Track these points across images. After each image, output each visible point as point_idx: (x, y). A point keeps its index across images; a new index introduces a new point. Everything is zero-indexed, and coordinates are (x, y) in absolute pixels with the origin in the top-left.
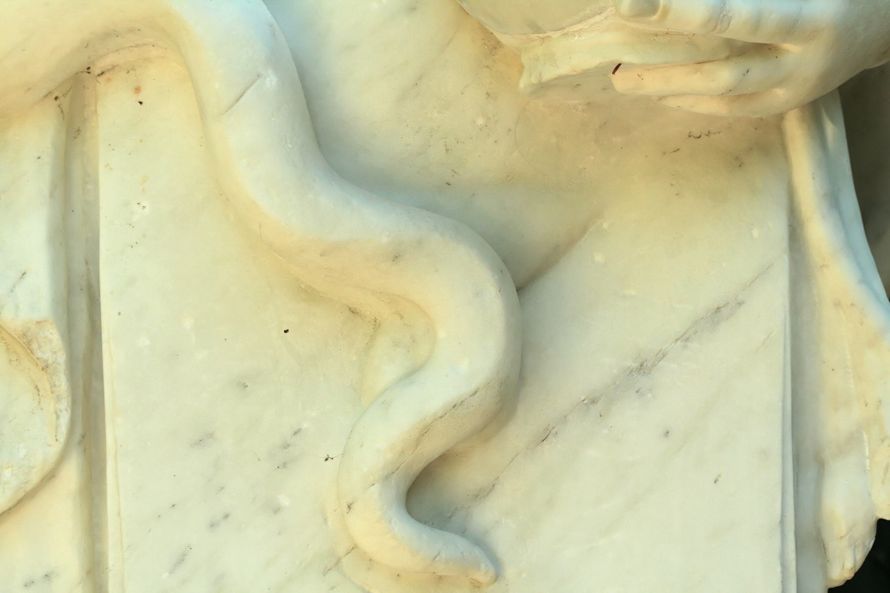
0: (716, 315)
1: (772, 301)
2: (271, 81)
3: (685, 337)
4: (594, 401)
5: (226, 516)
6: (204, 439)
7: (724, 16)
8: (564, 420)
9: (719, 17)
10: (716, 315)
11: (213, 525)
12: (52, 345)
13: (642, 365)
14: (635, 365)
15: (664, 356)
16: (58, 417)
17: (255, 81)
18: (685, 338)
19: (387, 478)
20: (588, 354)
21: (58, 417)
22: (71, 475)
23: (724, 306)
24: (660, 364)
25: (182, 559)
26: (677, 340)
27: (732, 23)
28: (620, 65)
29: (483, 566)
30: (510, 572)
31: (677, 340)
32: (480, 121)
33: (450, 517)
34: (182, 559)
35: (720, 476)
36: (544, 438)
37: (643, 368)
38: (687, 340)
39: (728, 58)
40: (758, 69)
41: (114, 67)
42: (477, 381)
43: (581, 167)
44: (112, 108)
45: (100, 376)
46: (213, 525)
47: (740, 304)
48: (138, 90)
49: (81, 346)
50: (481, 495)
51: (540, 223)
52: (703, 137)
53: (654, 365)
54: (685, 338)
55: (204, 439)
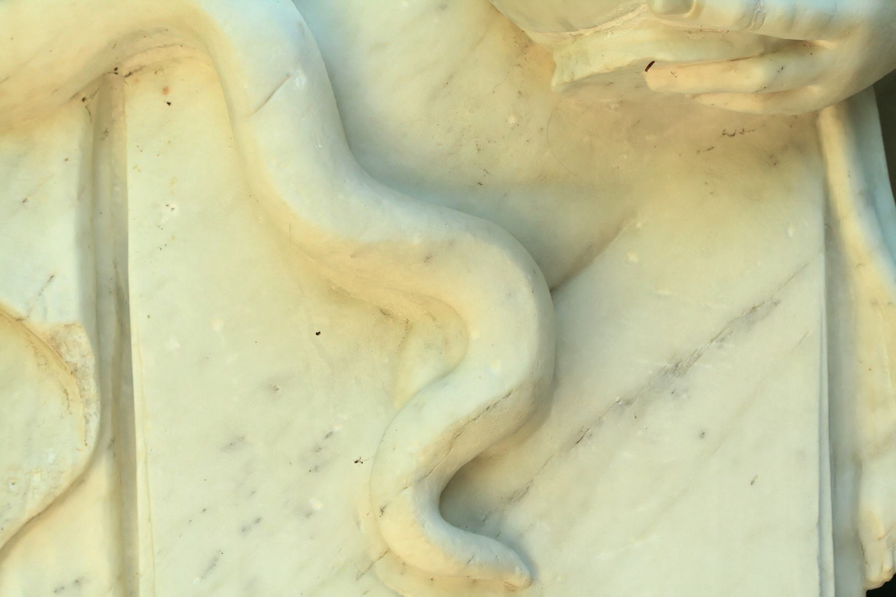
0: (752, 315)
1: (806, 305)
2: (300, 81)
4: (628, 403)
5: (258, 521)
6: (235, 443)
10: (752, 315)
11: (244, 530)
12: (81, 348)
13: (677, 366)
14: (670, 366)
15: (699, 356)
17: (284, 81)
18: (720, 339)
19: (420, 481)
20: (621, 356)
21: (87, 422)
22: (101, 480)
24: (696, 364)
25: (213, 564)
26: (712, 341)
27: (766, 19)
28: (653, 62)
29: (517, 569)
32: (512, 120)
34: (213, 564)
38: (723, 340)
39: (762, 55)
40: (793, 66)
41: (141, 68)
42: (510, 383)
44: (140, 109)
45: (130, 381)
46: (244, 530)
47: (776, 304)
48: (166, 90)
49: (110, 350)
50: (516, 497)
51: (573, 223)
52: (738, 135)
53: (689, 366)
54: (720, 339)
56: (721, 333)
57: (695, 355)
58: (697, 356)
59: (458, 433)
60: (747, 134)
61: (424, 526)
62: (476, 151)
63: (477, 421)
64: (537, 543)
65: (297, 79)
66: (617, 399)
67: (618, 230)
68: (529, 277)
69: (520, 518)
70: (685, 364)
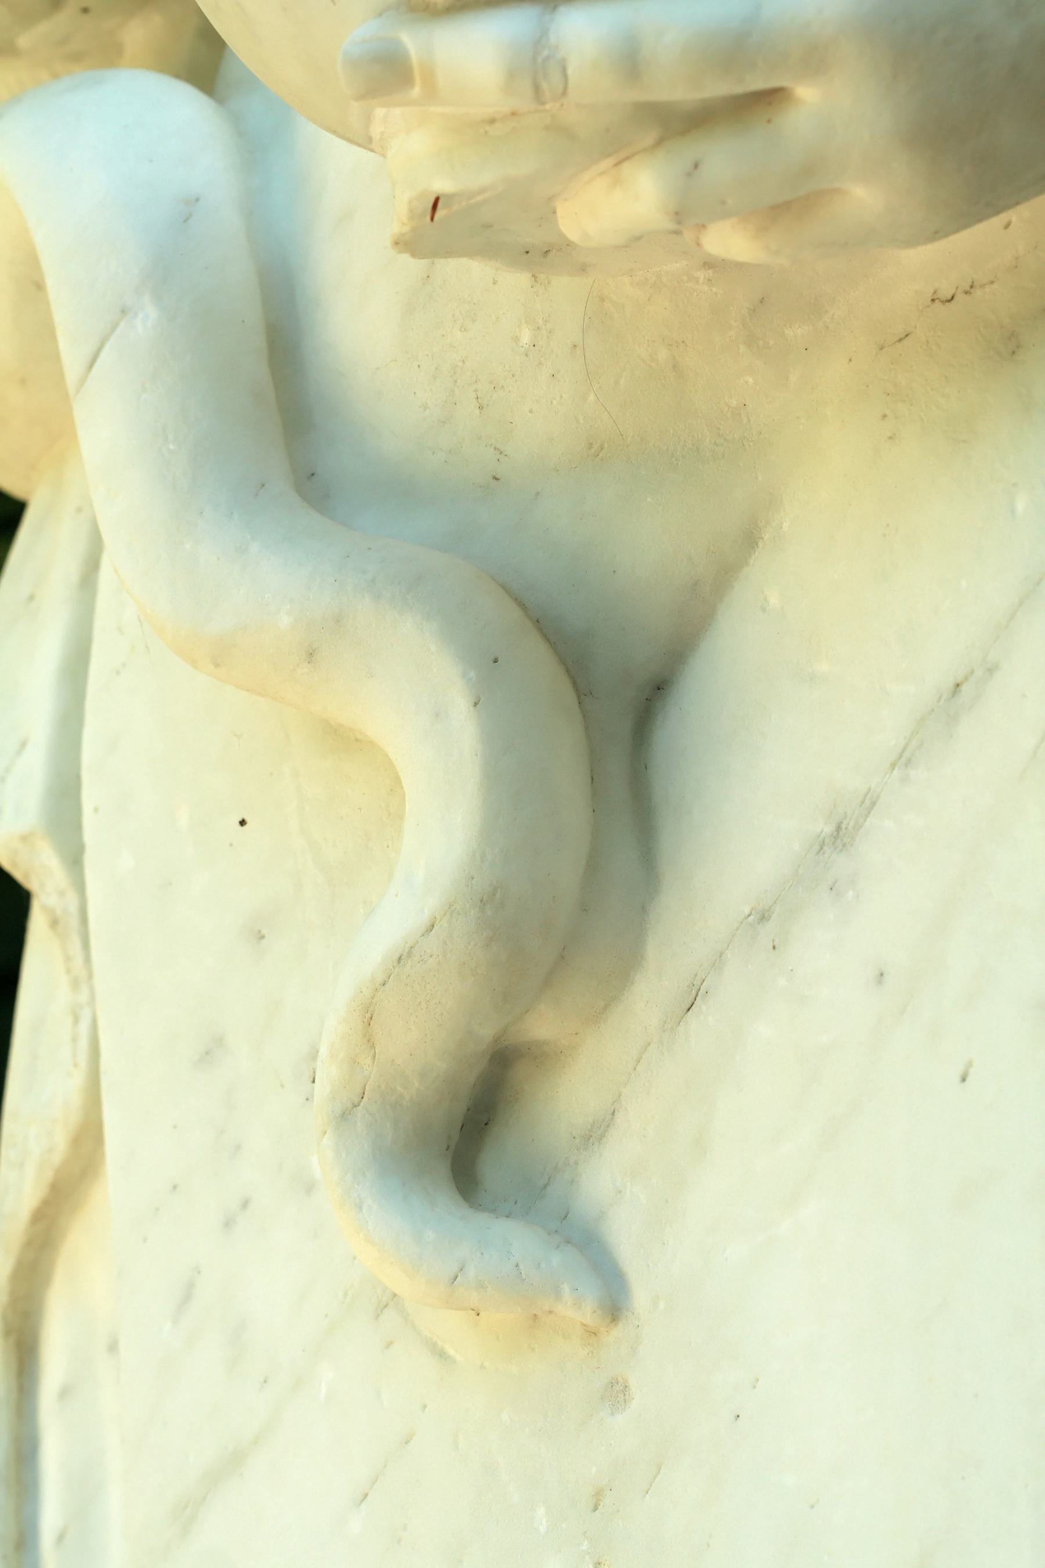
2: (147, 318)
3: (903, 760)
4: (764, 917)
5: (245, 1204)
7: (546, 60)
8: (718, 961)
9: (630, 61)
13: (839, 828)
14: (829, 829)
15: (874, 804)
16: (76, 1020)
17: (114, 327)
18: (903, 760)
19: (344, 1116)
21: (76, 1020)
23: (966, 679)
24: (867, 823)
25: (187, 1297)
26: (893, 766)
27: (570, 71)
28: (437, 200)
29: (566, 1288)
30: (641, 1296)
31: (893, 766)
32: (526, 337)
33: (545, 1187)
34: (187, 1297)
35: (970, 1064)
36: (691, 1001)
37: (840, 836)
38: (908, 763)
39: (659, 143)
42: (431, 905)
43: (734, 403)
46: (228, 1224)
47: (991, 670)
50: (594, 1135)
51: (647, 542)
52: (960, 298)
53: (858, 827)
54: (903, 760)
55: (211, 1052)
56: (904, 750)
57: (868, 802)
58: (869, 803)
59: (368, 1015)
60: (978, 293)
61: (361, 1208)
62: (477, 411)
63: (387, 986)
64: (626, 1237)
65: (140, 316)
66: (747, 912)
67: (750, 540)
68: (472, 674)
69: (613, 1185)
70: (852, 823)
